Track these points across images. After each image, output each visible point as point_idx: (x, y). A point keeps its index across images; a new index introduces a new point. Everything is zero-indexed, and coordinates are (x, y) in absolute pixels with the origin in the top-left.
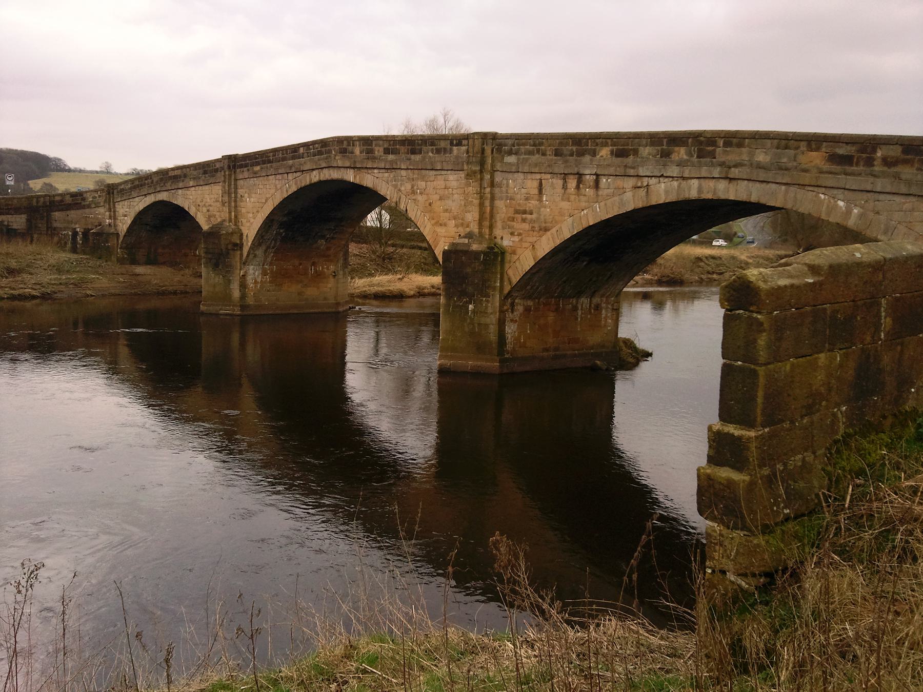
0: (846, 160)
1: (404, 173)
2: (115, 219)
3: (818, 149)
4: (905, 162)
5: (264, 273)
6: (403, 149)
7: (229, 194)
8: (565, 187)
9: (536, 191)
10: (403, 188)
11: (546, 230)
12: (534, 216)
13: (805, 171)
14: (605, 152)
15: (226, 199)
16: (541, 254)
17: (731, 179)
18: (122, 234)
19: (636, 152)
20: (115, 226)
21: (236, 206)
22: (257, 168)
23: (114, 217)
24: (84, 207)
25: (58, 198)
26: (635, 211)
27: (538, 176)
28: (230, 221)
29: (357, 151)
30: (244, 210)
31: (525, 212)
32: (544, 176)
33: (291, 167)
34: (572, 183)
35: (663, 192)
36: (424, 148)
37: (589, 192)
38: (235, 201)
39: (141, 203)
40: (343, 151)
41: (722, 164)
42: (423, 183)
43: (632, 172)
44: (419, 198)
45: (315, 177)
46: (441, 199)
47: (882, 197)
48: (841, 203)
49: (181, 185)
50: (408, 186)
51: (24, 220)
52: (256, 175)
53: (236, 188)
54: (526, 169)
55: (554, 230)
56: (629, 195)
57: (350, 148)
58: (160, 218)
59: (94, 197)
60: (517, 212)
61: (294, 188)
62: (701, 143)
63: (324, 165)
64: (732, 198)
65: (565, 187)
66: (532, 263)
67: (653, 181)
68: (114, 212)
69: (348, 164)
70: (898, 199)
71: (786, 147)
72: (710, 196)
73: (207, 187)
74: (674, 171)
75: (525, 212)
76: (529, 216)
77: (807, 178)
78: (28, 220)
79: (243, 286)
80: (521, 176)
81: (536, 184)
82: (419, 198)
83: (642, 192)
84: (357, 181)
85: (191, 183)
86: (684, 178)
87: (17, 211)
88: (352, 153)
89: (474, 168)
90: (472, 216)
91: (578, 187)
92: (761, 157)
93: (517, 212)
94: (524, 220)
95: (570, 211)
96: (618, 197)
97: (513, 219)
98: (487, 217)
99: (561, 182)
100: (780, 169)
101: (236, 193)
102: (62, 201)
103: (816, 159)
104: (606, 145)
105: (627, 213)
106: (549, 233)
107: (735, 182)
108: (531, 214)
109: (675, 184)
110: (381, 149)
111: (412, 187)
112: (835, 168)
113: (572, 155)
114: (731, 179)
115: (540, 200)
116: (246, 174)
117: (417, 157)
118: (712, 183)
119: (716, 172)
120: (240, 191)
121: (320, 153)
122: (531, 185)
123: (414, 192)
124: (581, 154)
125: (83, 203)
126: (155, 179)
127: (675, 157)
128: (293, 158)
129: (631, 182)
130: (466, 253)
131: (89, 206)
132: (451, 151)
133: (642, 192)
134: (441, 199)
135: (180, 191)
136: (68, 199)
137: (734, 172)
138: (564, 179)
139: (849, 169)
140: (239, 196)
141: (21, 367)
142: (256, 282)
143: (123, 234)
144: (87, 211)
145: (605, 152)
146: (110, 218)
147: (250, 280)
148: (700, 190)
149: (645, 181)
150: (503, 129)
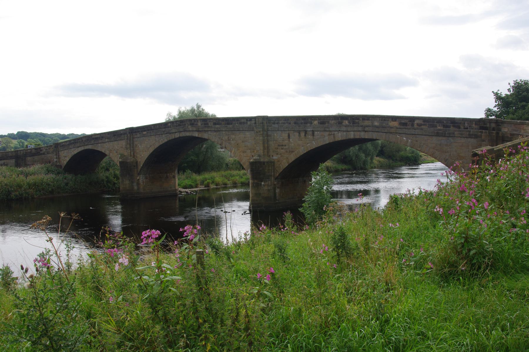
0: (405, 124)
1: (224, 132)
2: (59, 158)
3: (395, 121)
4: (424, 125)
5: (146, 178)
6: (223, 123)
7: (130, 145)
8: (300, 135)
9: (287, 138)
10: (223, 138)
11: (292, 152)
12: (287, 147)
13: (392, 128)
14: (316, 122)
15: (128, 146)
16: (290, 161)
17: (366, 131)
18: (63, 167)
19: (328, 123)
20: (59, 162)
21: (133, 150)
22: (145, 133)
23: (59, 158)
24: (41, 154)
25: (29, 151)
26: (330, 144)
27: (288, 132)
28: (131, 156)
29: (199, 124)
30: (137, 151)
31: (282, 146)
32: (290, 132)
33: (164, 132)
34: (303, 134)
35: (340, 136)
36: (234, 122)
37: (310, 137)
38: (133, 147)
39: (75, 151)
40: (192, 124)
41: (362, 126)
42: (234, 136)
43: (327, 129)
44: (232, 142)
45: (177, 135)
46: (243, 142)
47: (417, 136)
48: (404, 138)
49: (100, 141)
50: (226, 137)
51: (14, 162)
52: (144, 136)
53: (133, 142)
54: (282, 129)
55: (296, 152)
56: (327, 138)
57: (196, 123)
58: (85, 156)
59: (46, 150)
60: (279, 146)
61: (166, 140)
62: (353, 119)
63: (182, 130)
64: (366, 137)
65: (300, 135)
66: (287, 165)
67: (336, 133)
68: (59, 155)
69: (195, 130)
70: (423, 136)
71: (385, 120)
72: (358, 137)
73: (116, 142)
74: (344, 129)
75: (282, 146)
76: (285, 147)
77: (393, 130)
78: (16, 162)
79: (138, 184)
80: (280, 132)
81: (287, 135)
82: (232, 142)
83: (332, 137)
84: (200, 136)
85: (107, 140)
86: (348, 131)
87: (11, 158)
88: (197, 125)
89: (259, 130)
90: (260, 148)
91: (305, 135)
92: (376, 124)
93: (279, 146)
94: (282, 149)
95: (302, 145)
96: (323, 139)
97: (277, 149)
98: (266, 148)
99: (298, 134)
100: (383, 127)
101: (133, 144)
102: (31, 152)
103: (395, 124)
104: (316, 120)
105: (326, 144)
106: (294, 153)
107: (367, 133)
108: (285, 146)
109: (345, 133)
110: (212, 123)
111: (228, 138)
112: (402, 127)
113: (302, 124)
114: (366, 131)
115: (289, 141)
116: (138, 135)
117: (231, 126)
118: (359, 133)
119: (360, 129)
120: (135, 143)
121: (179, 125)
122: (285, 135)
123: (229, 140)
124: (306, 123)
125: (41, 152)
126: (84, 139)
127: (344, 124)
128: (165, 128)
129: (327, 133)
130: (260, 163)
131: (44, 154)
132: (247, 123)
133: (332, 137)
134: (243, 142)
135: (100, 145)
136: (34, 151)
137: (366, 129)
138: (299, 133)
139: (406, 127)
140: (135, 145)
141: (9, 232)
142: (143, 182)
143: (64, 165)
144: (43, 156)
145: (316, 122)
146: (57, 158)
147: (141, 181)
148: (354, 135)
149: (333, 133)
150: (270, 115)
